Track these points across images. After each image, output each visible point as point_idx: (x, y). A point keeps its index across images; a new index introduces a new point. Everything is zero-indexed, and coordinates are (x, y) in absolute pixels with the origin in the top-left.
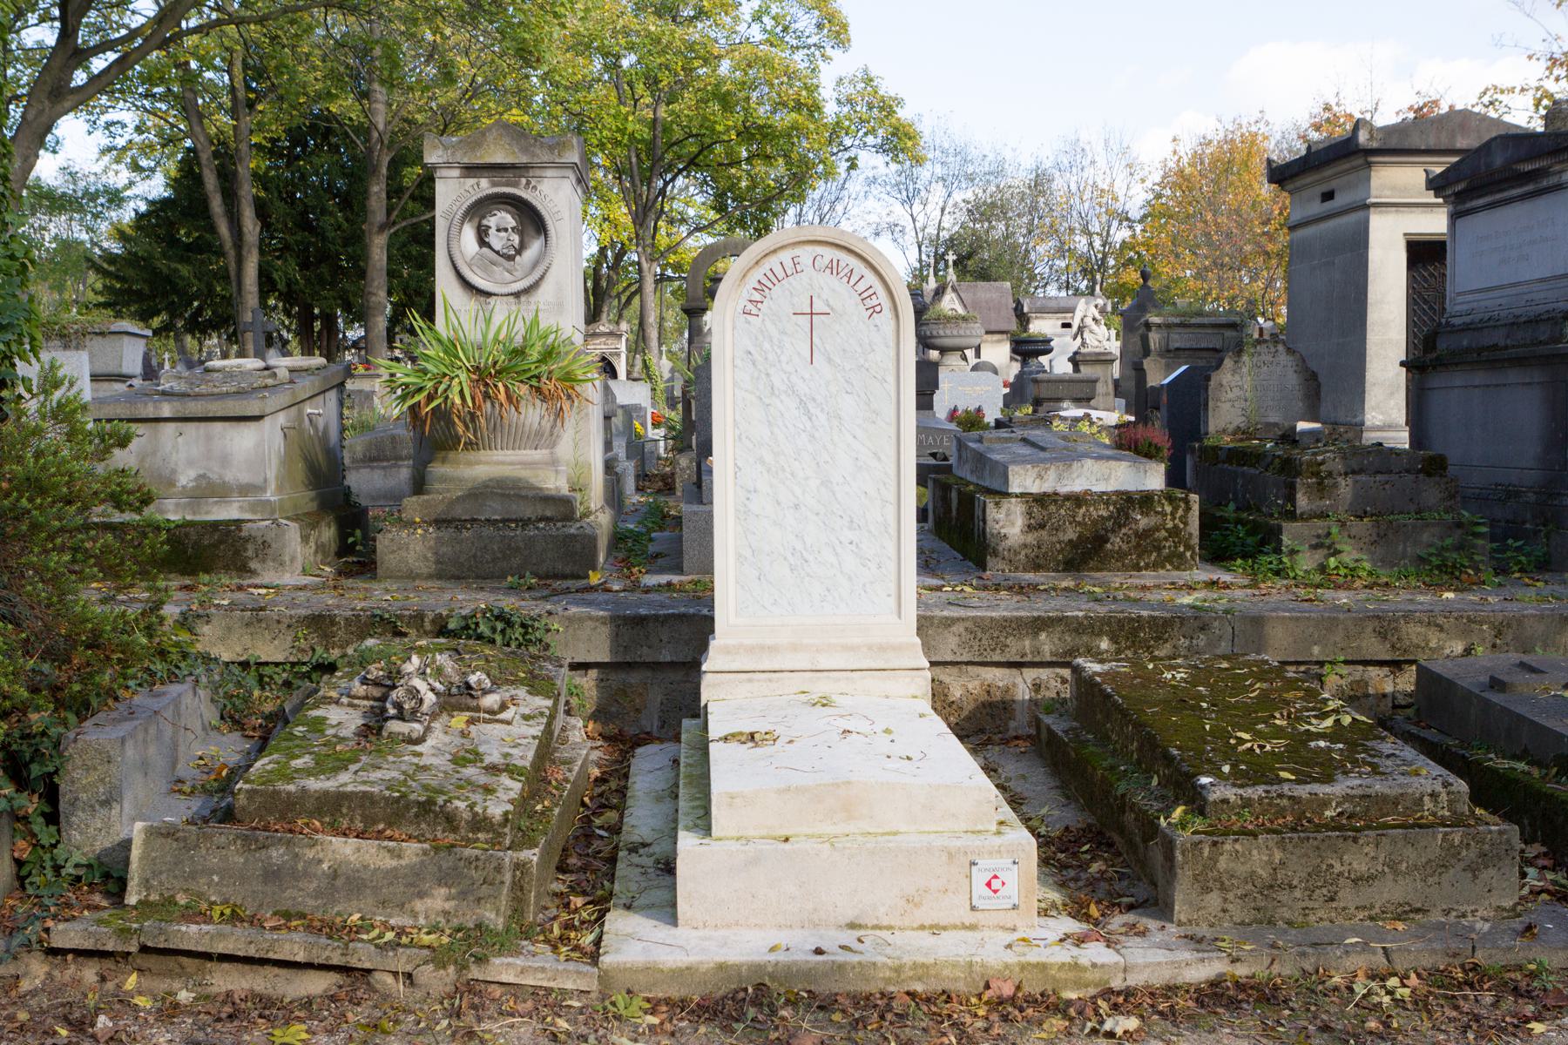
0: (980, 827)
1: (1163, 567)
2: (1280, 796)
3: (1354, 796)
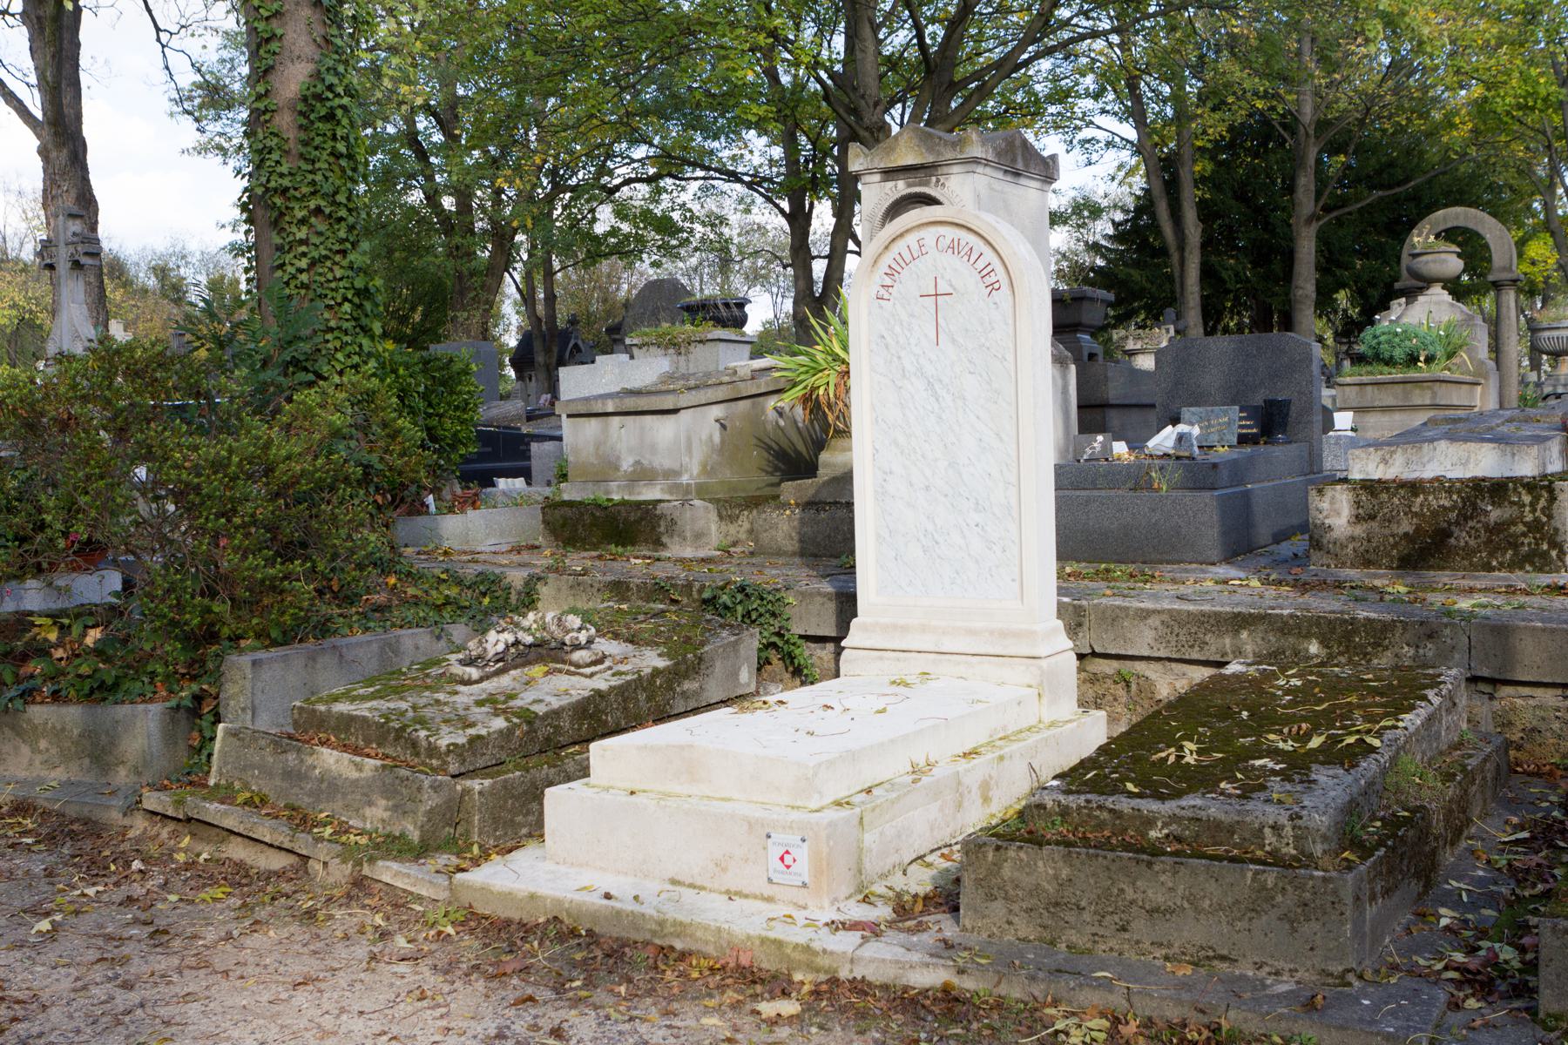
0: (799, 803)
1: (1521, 568)
2: (1100, 807)
3: (1182, 818)
